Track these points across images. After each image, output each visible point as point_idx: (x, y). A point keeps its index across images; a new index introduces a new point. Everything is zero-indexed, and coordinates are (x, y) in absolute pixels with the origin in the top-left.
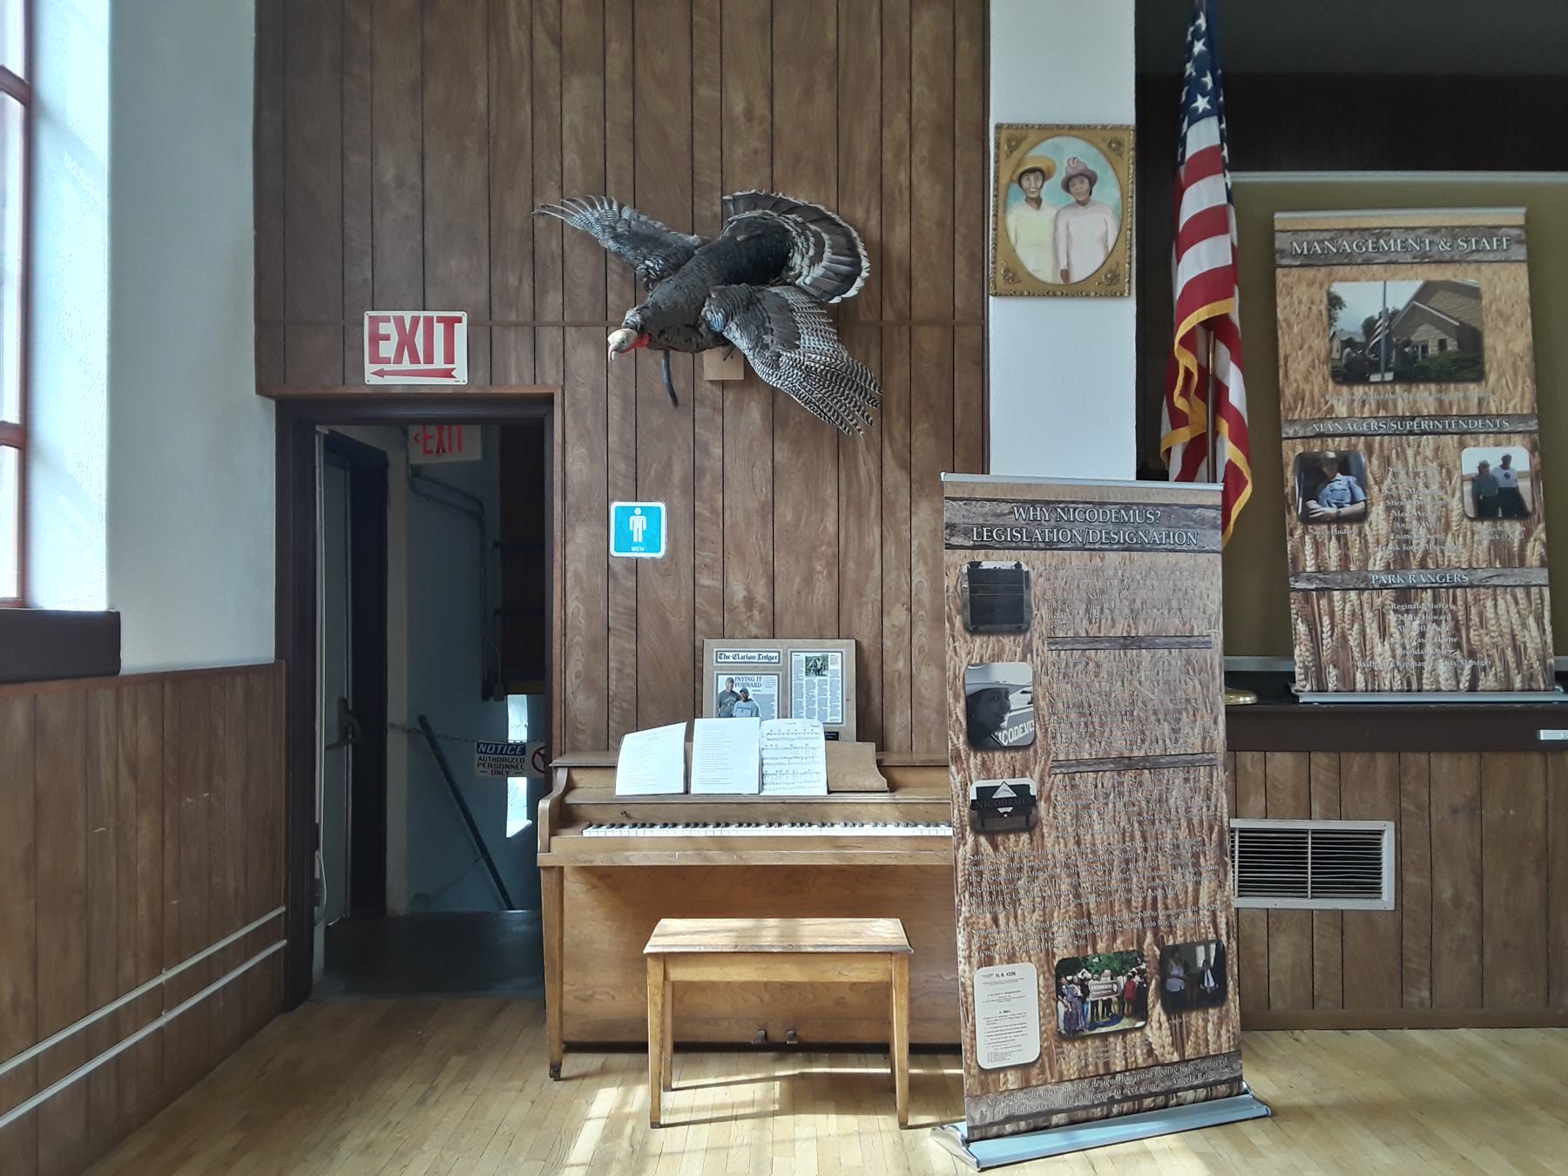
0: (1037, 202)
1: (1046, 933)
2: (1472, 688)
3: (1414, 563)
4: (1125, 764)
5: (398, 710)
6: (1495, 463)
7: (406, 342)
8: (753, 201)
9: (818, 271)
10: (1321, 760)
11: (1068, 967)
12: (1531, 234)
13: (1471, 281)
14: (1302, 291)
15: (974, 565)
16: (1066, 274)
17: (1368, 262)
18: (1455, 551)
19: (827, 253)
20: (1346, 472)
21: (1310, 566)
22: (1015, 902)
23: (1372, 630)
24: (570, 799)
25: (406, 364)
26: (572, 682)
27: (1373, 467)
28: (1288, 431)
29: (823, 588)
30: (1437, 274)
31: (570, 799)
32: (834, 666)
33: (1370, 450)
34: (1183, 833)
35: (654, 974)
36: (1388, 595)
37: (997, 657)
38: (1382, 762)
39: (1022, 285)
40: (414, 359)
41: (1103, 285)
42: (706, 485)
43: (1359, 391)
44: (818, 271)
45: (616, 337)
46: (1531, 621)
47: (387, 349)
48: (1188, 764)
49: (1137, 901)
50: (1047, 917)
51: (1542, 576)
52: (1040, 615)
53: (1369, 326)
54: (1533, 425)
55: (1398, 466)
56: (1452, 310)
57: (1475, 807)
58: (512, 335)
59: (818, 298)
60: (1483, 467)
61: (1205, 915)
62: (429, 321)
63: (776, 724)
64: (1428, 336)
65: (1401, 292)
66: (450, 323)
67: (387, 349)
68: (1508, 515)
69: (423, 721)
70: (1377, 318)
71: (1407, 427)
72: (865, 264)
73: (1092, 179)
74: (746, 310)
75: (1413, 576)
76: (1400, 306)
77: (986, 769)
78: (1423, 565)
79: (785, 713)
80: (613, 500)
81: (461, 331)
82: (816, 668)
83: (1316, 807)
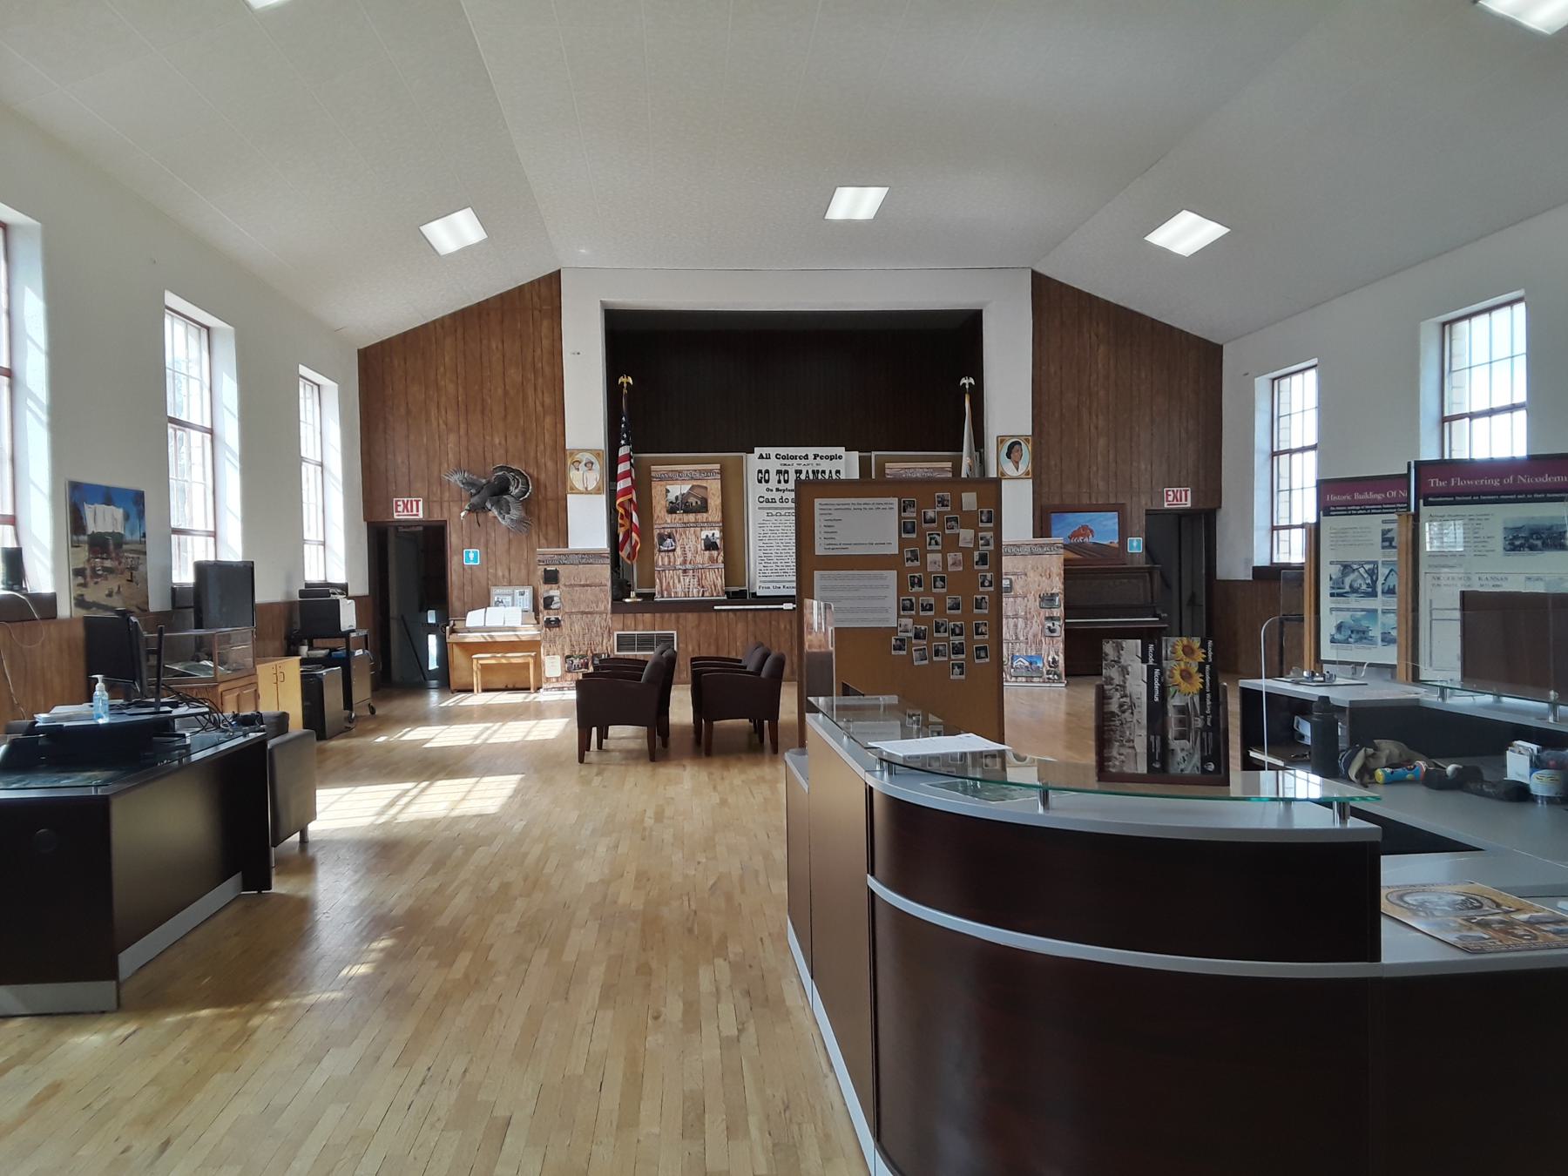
0: (578, 469)
1: (563, 649)
2: (703, 596)
3: (688, 563)
4: (583, 613)
5: (394, 611)
6: (710, 535)
7: (1175, 497)
8: (502, 468)
9: (517, 491)
10: (658, 615)
11: (568, 657)
12: (722, 472)
13: (705, 485)
14: (659, 488)
15: (545, 569)
16: (586, 489)
17: (677, 480)
18: (699, 559)
19: (520, 486)
20: (670, 538)
21: (660, 564)
22: (555, 642)
23: (676, 581)
24: (455, 627)
25: (405, 513)
26: (454, 599)
27: (677, 537)
28: (655, 527)
29: (524, 572)
30: (695, 483)
31: (455, 627)
32: (527, 594)
33: (676, 532)
34: (599, 629)
35: (475, 661)
36: (680, 571)
37: (551, 589)
38: (673, 615)
39: (575, 491)
40: (408, 511)
41: (597, 491)
42: (491, 545)
43: (674, 515)
44: (517, 491)
45: (463, 514)
46: (719, 578)
47: (400, 509)
48: (601, 613)
49: (586, 643)
50: (563, 646)
51: (722, 566)
52: (562, 580)
53: (677, 498)
54: (721, 524)
55: (684, 536)
56: (701, 493)
57: (698, 626)
58: (435, 504)
59: (517, 498)
60: (707, 536)
61: (605, 648)
62: (411, 501)
63: (510, 608)
64: (692, 500)
65: (686, 488)
67: (400, 509)
68: (713, 550)
69: (402, 617)
71: (686, 525)
72: (530, 487)
73: (592, 464)
74: (497, 504)
75: (688, 566)
76: (685, 492)
77: (548, 614)
78: (690, 563)
79: (513, 605)
81: (421, 504)
82: (522, 594)
83: (656, 628)
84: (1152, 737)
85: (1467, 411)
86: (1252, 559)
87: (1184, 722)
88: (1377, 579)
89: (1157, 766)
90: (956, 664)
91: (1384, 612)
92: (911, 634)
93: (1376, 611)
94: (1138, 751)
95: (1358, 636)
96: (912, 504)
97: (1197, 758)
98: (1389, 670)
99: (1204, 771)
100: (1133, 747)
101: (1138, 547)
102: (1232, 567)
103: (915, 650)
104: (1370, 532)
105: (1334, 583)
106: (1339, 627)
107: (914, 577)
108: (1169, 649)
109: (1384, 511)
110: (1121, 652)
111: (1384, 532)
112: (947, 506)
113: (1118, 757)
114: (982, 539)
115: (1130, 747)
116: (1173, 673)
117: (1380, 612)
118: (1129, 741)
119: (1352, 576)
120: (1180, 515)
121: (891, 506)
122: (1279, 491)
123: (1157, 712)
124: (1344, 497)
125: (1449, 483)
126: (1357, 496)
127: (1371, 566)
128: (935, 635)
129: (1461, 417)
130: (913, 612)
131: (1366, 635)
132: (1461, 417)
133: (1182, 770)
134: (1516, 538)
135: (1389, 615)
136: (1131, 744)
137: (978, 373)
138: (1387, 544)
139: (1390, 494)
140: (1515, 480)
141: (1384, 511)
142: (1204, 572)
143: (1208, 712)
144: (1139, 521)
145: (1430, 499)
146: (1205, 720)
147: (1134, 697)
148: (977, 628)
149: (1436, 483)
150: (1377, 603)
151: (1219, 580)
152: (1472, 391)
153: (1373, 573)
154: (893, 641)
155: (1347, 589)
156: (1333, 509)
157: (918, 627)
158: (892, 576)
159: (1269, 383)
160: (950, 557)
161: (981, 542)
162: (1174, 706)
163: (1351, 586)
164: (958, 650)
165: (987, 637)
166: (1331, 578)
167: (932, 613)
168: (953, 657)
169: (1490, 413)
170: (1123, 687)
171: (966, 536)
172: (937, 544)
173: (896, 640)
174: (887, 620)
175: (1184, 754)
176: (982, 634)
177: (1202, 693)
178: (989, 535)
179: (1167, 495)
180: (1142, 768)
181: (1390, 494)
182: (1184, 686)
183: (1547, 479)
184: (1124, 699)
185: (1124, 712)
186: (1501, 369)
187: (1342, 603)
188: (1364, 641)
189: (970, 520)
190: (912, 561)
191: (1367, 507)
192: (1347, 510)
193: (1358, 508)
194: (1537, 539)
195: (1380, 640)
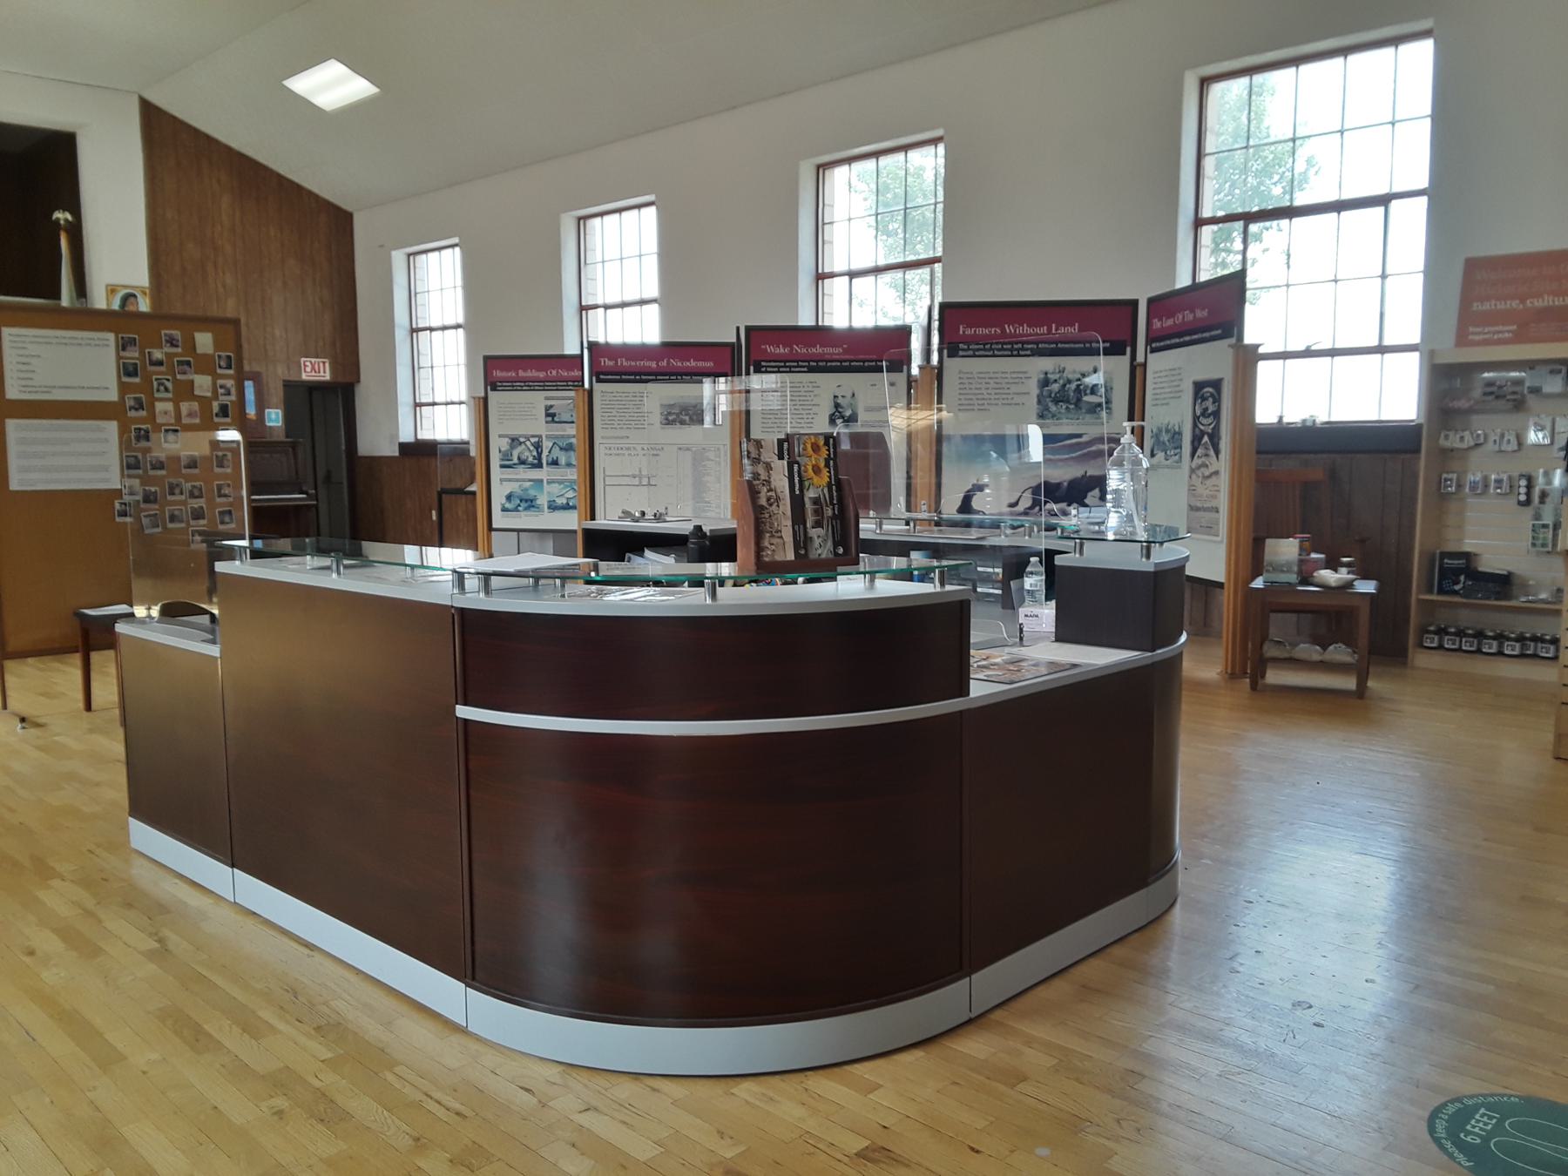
7: (313, 368)
40: (315, 372)
47: (308, 369)
66: (324, 363)
67: (308, 369)
70: (1119, 515)
80: (125, 394)
81: (327, 365)
84: (796, 527)
85: (428, 325)
86: (397, 435)
87: (818, 512)
88: (542, 450)
89: (803, 552)
90: (197, 531)
91: (549, 482)
92: (139, 497)
93: (542, 481)
94: (785, 540)
95: (526, 505)
96: (133, 342)
97: (830, 544)
98: (551, 534)
99: (836, 554)
100: (781, 537)
101: (277, 421)
102: (375, 442)
103: (144, 516)
104: (534, 407)
105: (504, 455)
106: (509, 497)
107: (140, 429)
108: (802, 446)
109: (546, 388)
110: (761, 450)
111: (548, 408)
112: (177, 346)
113: (769, 547)
114: (221, 387)
115: (778, 537)
116: (807, 469)
117: (545, 482)
118: (777, 532)
119: (520, 449)
120: (314, 388)
121: (106, 342)
122: (419, 368)
123: (797, 503)
124: (510, 374)
125: (617, 362)
126: (521, 373)
127: (536, 439)
128: (169, 497)
129: (595, 307)
130: (140, 472)
131: (533, 504)
132: (595, 307)
133: (819, 555)
134: (669, 414)
135: (554, 485)
136: (779, 534)
137: (75, 207)
138: (550, 419)
139: (551, 373)
140: (668, 363)
141: (546, 388)
142: (343, 447)
143: (835, 502)
144: (276, 392)
145: (602, 377)
146: (834, 509)
147: (779, 491)
148: (220, 488)
149: (607, 363)
150: (543, 474)
151: (361, 457)
152: (605, 284)
153: (538, 446)
154: (117, 506)
155: (515, 460)
156: (500, 384)
157: (147, 488)
158: (112, 427)
159: (405, 258)
160: (185, 407)
161: (221, 391)
162: (810, 498)
163: (519, 458)
164: (198, 514)
165: (231, 499)
166: (500, 451)
167: (163, 472)
168: (192, 522)
169: (444, 328)
170: (769, 482)
171: (202, 383)
172: (167, 390)
173: (121, 504)
174: (107, 480)
175: (820, 539)
176: (226, 496)
177: (829, 485)
178: (230, 383)
179: (305, 366)
180: (791, 556)
181: (551, 373)
182: (816, 480)
183: (693, 363)
184: (770, 494)
185: (771, 505)
186: (631, 265)
187: (509, 473)
188: (533, 509)
189: (205, 365)
190: (136, 409)
191: (531, 384)
192: (513, 386)
193: (523, 384)
194: (686, 415)
195: (546, 507)
